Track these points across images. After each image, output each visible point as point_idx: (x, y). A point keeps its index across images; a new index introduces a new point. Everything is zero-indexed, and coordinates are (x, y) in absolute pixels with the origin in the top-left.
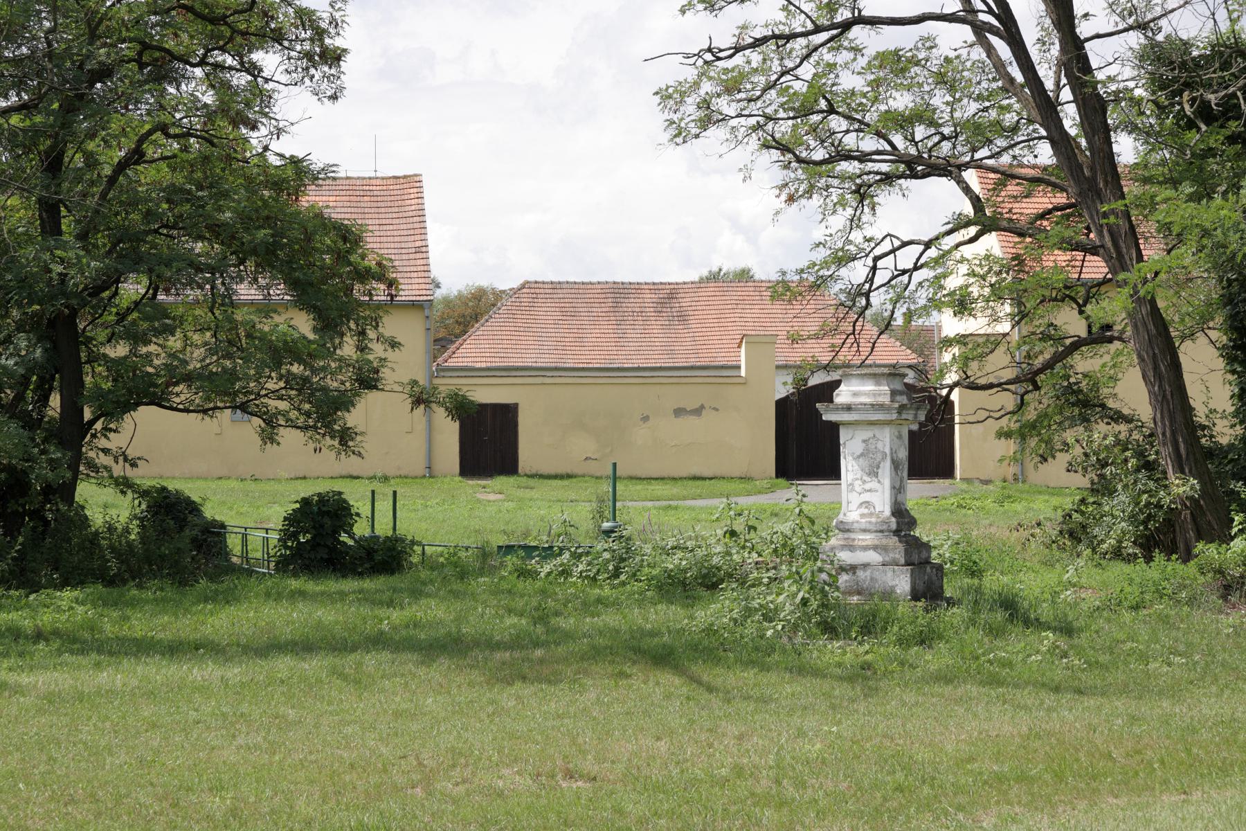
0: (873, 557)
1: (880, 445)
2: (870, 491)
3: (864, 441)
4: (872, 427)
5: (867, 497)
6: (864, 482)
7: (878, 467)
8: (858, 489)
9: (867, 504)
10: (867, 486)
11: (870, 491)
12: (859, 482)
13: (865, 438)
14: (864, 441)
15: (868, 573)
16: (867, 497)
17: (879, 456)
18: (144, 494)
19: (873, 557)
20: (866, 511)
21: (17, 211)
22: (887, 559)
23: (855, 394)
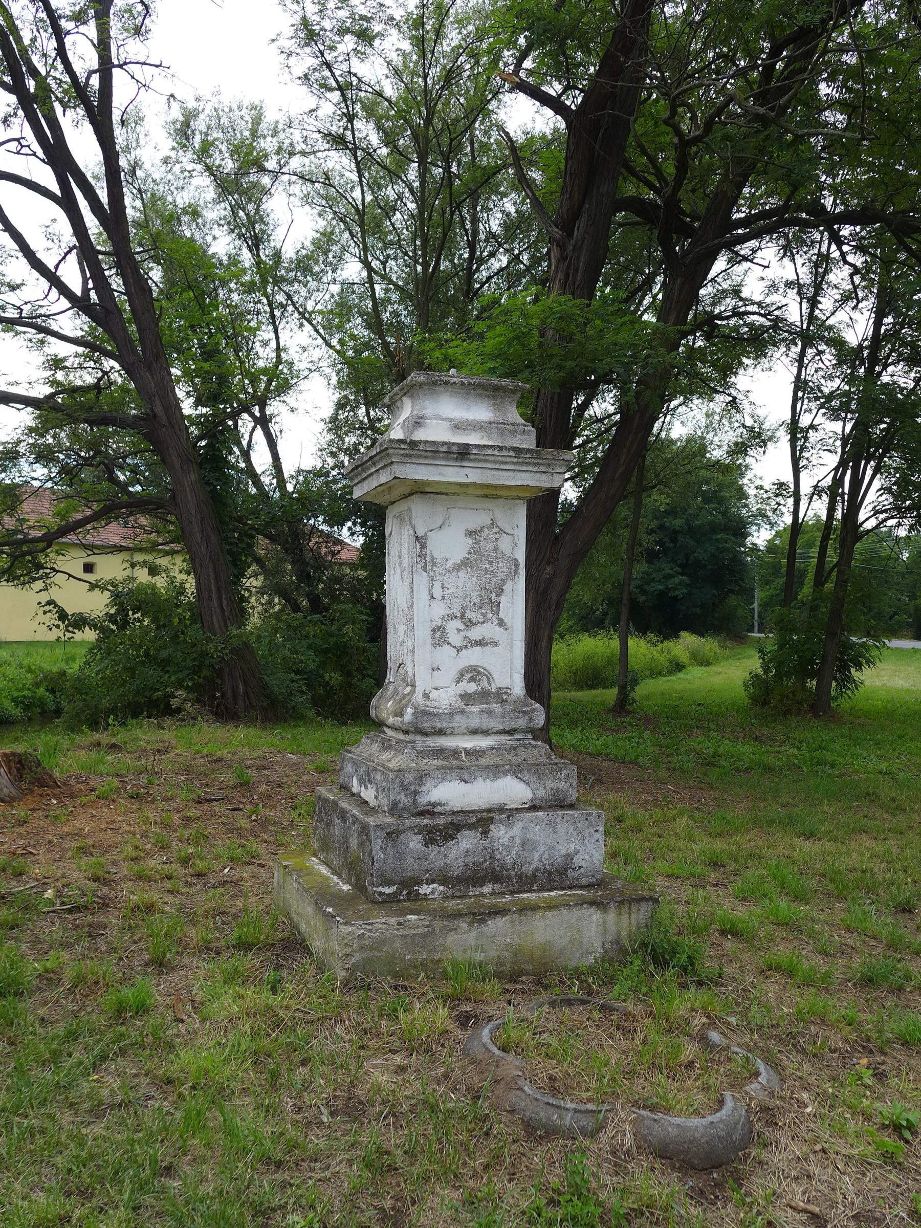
0: (512, 790)
1: (505, 544)
2: (481, 643)
3: (470, 533)
4: (488, 504)
5: (473, 656)
6: (469, 624)
7: (500, 591)
8: (455, 639)
9: (474, 673)
10: (476, 633)
11: (481, 643)
12: (458, 624)
13: (472, 526)
14: (470, 533)
15: (517, 830)
16: (473, 656)
17: (503, 567)
18: (387, 507)
19: (512, 790)
20: (472, 688)
21: (4, 1152)
22: (541, 793)
23: (459, 426)
